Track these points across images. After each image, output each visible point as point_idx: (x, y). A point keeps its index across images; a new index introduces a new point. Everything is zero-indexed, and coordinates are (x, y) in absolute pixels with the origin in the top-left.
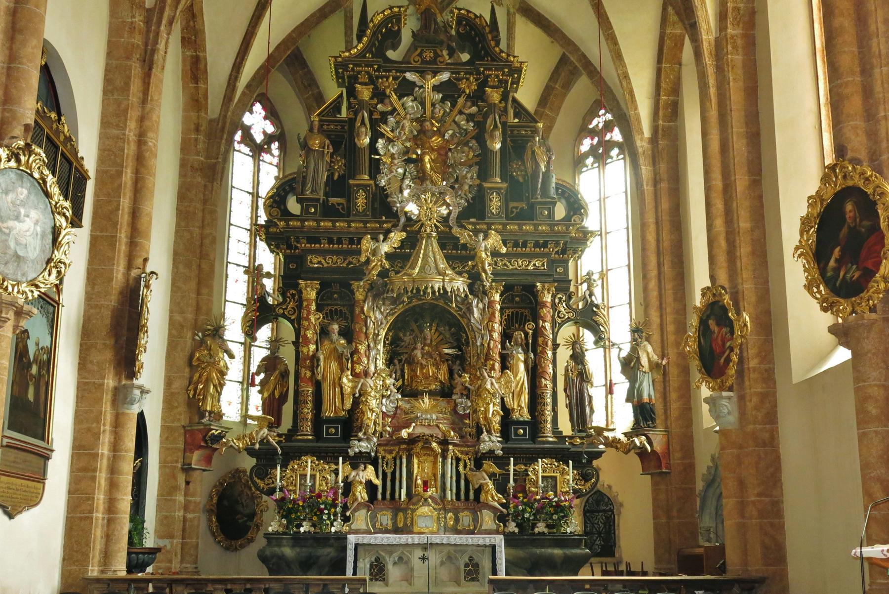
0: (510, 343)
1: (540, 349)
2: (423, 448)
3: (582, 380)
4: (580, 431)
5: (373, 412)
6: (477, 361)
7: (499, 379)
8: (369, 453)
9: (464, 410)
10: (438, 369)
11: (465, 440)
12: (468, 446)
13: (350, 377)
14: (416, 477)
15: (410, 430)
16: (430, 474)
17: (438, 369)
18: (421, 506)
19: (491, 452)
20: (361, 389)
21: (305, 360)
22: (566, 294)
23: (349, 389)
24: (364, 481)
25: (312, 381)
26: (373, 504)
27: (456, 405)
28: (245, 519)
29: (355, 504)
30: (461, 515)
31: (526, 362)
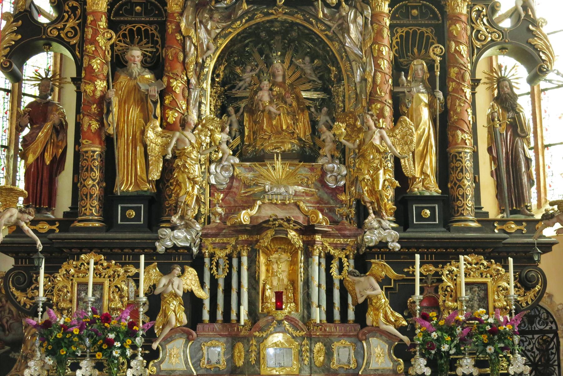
0: (406, 77)
1: (452, 86)
2: (274, 240)
3: (515, 134)
4: (513, 212)
5: (195, 183)
6: (356, 105)
7: (393, 130)
8: (189, 249)
9: (337, 181)
10: (296, 121)
11: (339, 226)
12: (344, 236)
13: (159, 129)
14: (264, 285)
15: (254, 212)
16: (286, 281)
17: (296, 121)
18: (272, 333)
19: (383, 244)
20: (176, 148)
21: (90, 104)
22: (487, 6)
23: (157, 148)
24: (180, 293)
25: (100, 137)
26: (195, 329)
27: (324, 173)
28: (7, 348)
29: (167, 330)
30: (336, 346)
31: (430, 106)
